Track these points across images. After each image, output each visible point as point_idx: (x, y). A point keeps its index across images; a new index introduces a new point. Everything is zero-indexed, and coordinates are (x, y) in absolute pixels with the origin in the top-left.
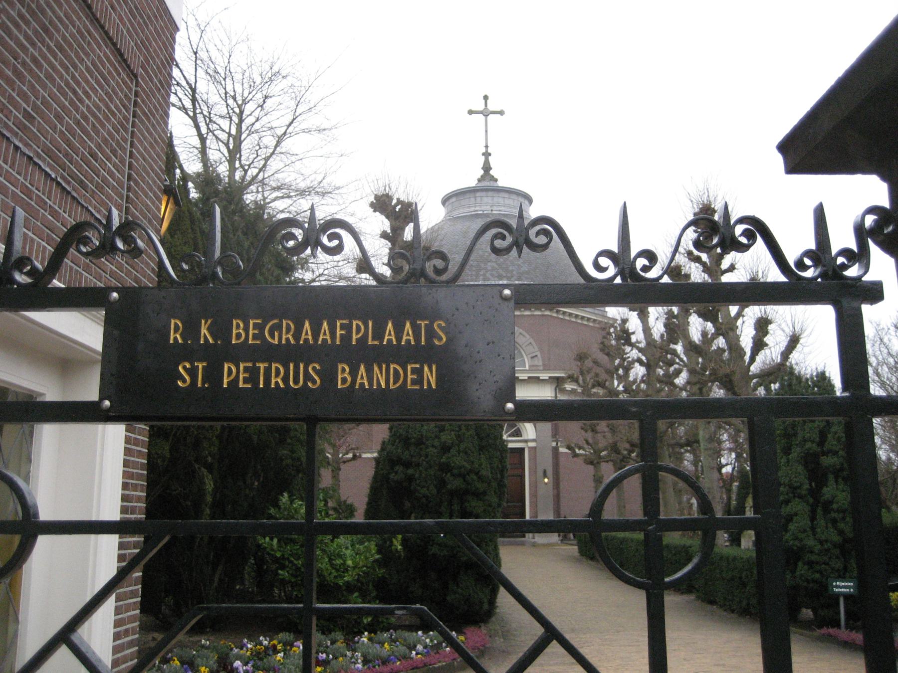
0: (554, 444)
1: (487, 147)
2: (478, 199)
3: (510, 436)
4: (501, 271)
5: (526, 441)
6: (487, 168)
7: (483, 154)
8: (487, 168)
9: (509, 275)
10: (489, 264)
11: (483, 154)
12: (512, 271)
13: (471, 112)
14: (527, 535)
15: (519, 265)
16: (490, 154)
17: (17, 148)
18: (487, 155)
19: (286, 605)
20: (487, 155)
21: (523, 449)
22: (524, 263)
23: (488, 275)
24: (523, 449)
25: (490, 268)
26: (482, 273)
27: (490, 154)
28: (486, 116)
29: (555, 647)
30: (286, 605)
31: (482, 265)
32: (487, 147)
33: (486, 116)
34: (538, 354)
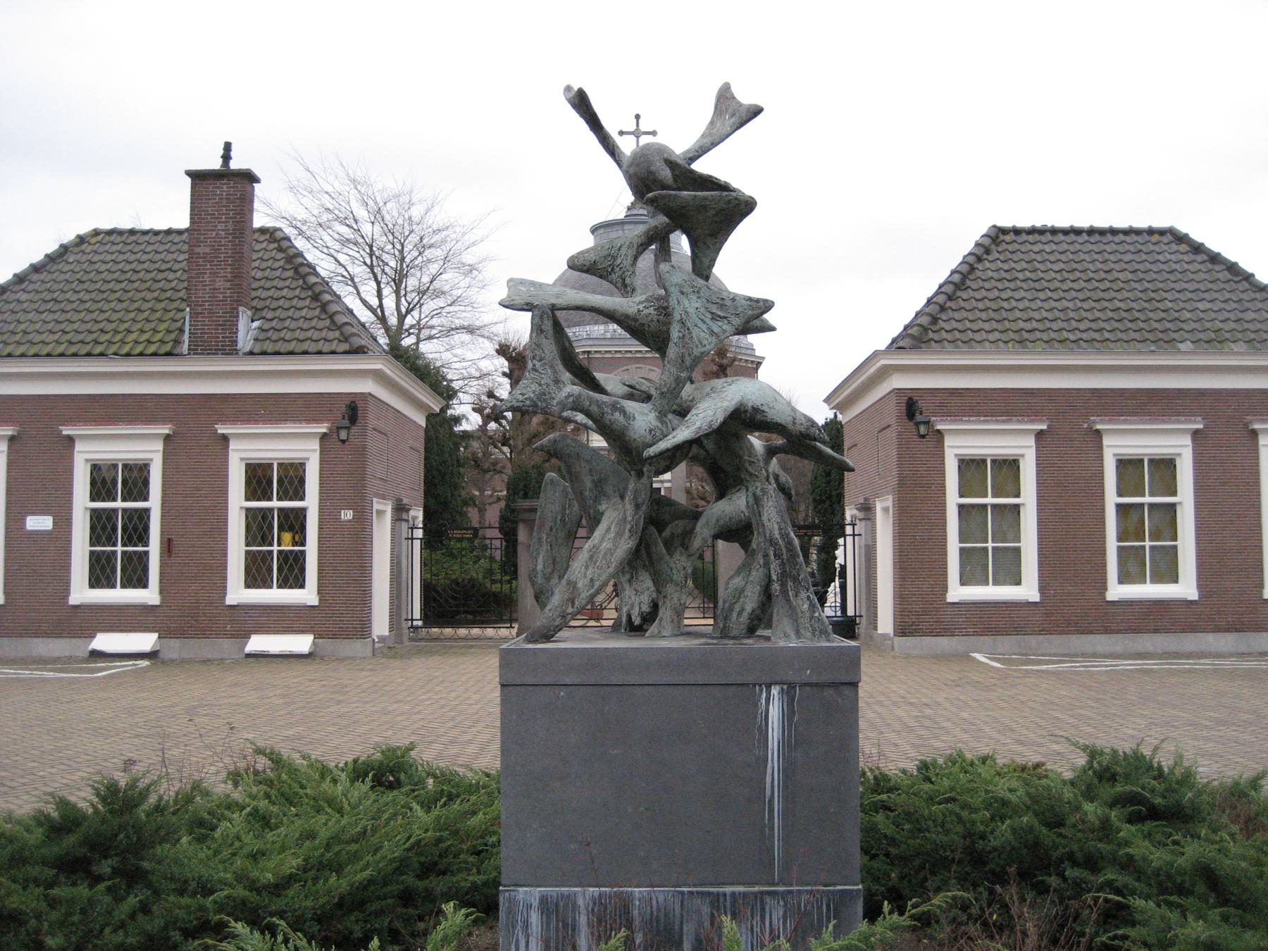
17: (181, 330)
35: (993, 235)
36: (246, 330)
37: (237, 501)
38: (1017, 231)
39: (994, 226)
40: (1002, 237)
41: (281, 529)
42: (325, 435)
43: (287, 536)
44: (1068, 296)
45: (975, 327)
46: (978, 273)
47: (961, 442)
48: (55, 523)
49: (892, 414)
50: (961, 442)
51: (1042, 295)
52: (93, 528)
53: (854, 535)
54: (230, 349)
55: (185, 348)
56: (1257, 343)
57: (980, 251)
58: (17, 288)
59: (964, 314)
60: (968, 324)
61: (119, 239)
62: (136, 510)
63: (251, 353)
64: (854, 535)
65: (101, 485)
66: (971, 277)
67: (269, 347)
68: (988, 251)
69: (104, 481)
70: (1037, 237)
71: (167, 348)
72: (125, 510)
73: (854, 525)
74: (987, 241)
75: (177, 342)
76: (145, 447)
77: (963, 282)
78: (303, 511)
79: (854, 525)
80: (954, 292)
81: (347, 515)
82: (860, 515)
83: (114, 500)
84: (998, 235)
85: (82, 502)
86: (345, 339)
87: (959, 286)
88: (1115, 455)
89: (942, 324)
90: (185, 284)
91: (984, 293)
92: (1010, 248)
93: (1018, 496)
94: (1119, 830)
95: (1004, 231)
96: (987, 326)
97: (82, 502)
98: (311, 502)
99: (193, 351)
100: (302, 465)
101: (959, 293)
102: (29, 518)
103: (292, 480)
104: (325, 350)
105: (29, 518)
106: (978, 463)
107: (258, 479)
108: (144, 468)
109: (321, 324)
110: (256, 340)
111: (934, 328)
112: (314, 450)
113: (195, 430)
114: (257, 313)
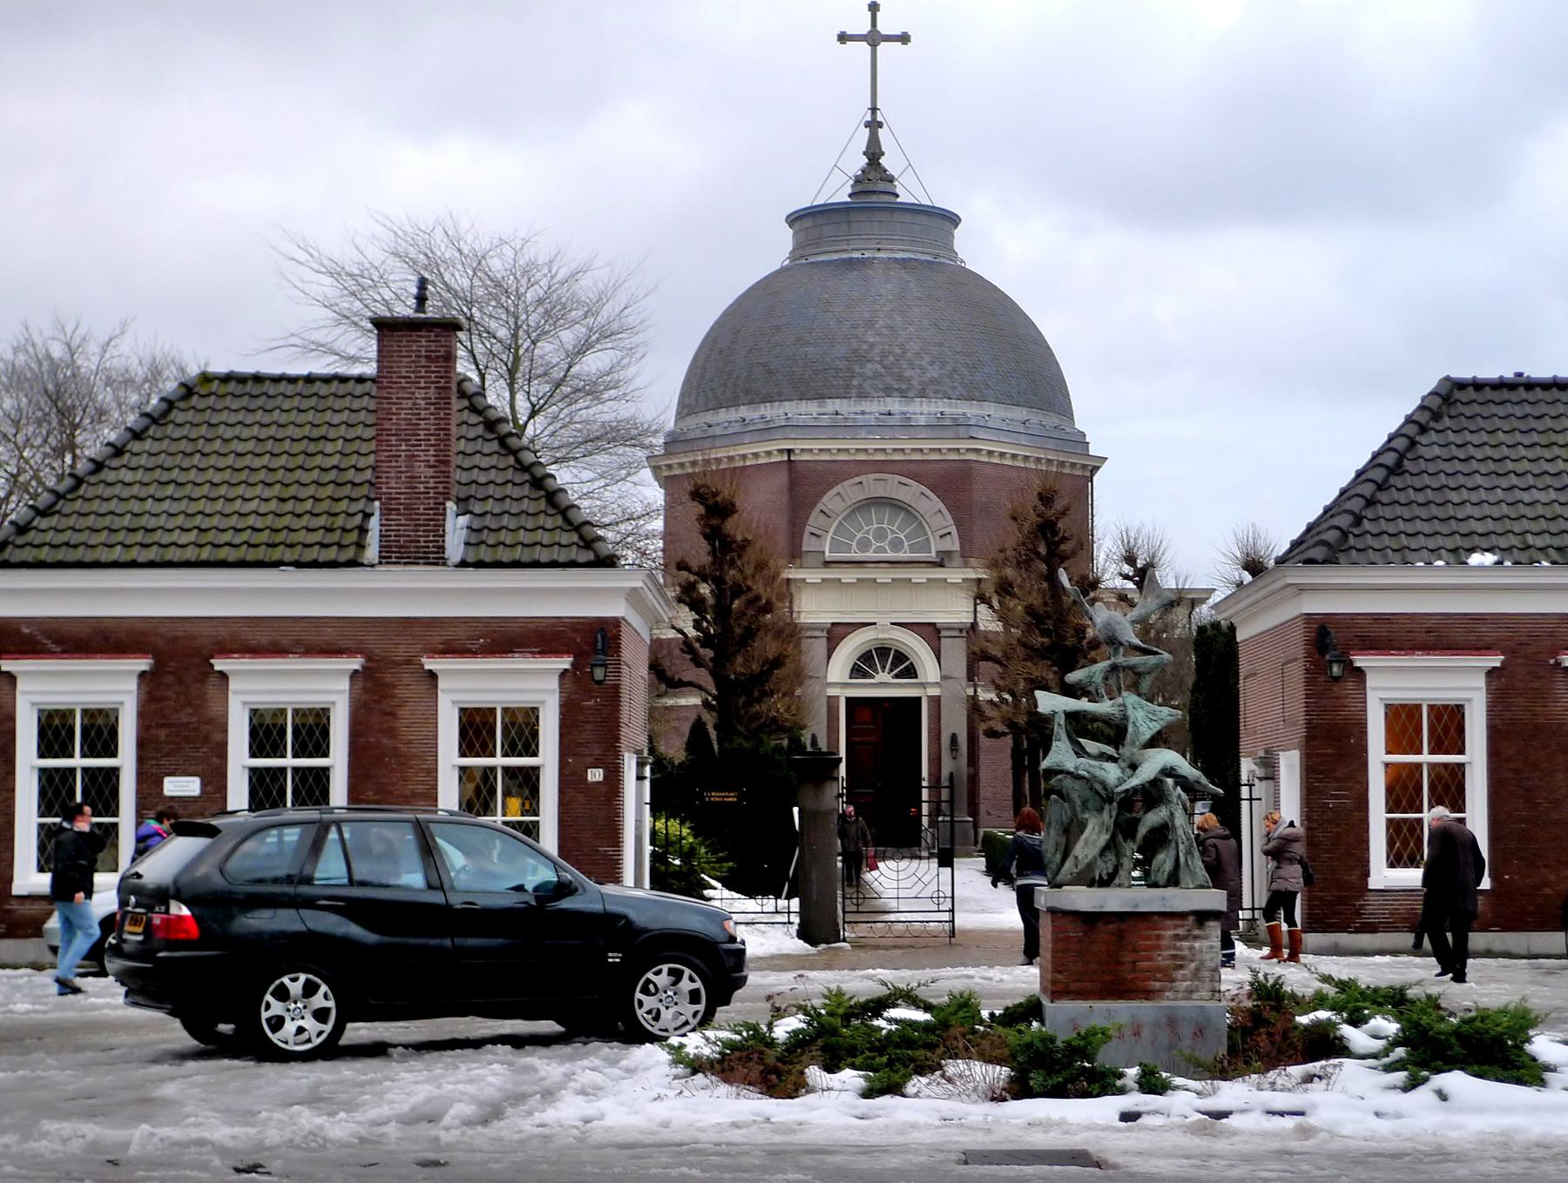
0: (970, 692)
1: (874, 110)
2: (854, 226)
3: (897, 676)
4: (890, 380)
5: (923, 685)
6: (874, 153)
7: (867, 125)
8: (874, 153)
9: (903, 386)
10: (869, 365)
11: (867, 125)
12: (909, 379)
13: (843, 38)
14: (881, 865)
15: (921, 368)
16: (880, 125)
17: (363, 530)
18: (874, 125)
19: (471, 942)
20: (874, 125)
21: (919, 699)
22: (932, 363)
23: (867, 386)
24: (919, 699)
25: (870, 374)
26: (855, 382)
27: (880, 125)
28: (874, 46)
29: (346, 881)
30: (471, 942)
31: (857, 369)
32: (874, 110)
33: (874, 46)
34: (953, 529)
35: (1444, 392)
36: (456, 528)
37: (449, 758)
38: (1478, 385)
39: (1447, 379)
40: (1458, 395)
41: (506, 794)
42: (356, 672)
43: (515, 803)
44: (1540, 483)
45: (1410, 528)
46: (1421, 450)
47: (1389, 682)
48: (203, 785)
49: (1296, 645)
50: (1389, 682)
51: (1504, 483)
52: (42, 793)
53: (1251, 799)
54: (435, 557)
55: (372, 553)
56: (1567, 556)
57: (1423, 418)
58: (115, 463)
59: (1399, 511)
60: (1401, 525)
61: (239, 389)
62: (310, 769)
63: (463, 564)
64: (1251, 799)
65: (265, 736)
66: (1410, 456)
67: (485, 554)
68: (1436, 416)
69: (100, 732)
70: (1506, 394)
71: (349, 554)
72: (296, 770)
73: (1251, 786)
74: (1437, 401)
75: (361, 546)
76: (326, 686)
77: (1399, 464)
78: (114, 772)
79: (1251, 786)
80: (1386, 479)
81: (596, 775)
82: (1259, 772)
83: (493, 755)
84: (1452, 399)
85: (239, 760)
86: (588, 543)
87: (1396, 470)
88: (454, 702)
89: (1367, 525)
90: (371, 459)
91: (1443, 479)
92: (1468, 411)
93: (1461, 751)
94: (126, 1146)
95: (1461, 385)
96: (1426, 528)
97: (239, 760)
98: (547, 758)
99: (386, 558)
100: (326, 711)
101: (1393, 480)
102: (167, 780)
103: (313, 733)
104: (141, 559)
105: (167, 780)
106: (1412, 711)
107: (55, 732)
108: (532, 715)
109: (549, 524)
110: (467, 544)
111: (1356, 531)
112: (1479, 689)
113: (181, 667)
114: (464, 505)
